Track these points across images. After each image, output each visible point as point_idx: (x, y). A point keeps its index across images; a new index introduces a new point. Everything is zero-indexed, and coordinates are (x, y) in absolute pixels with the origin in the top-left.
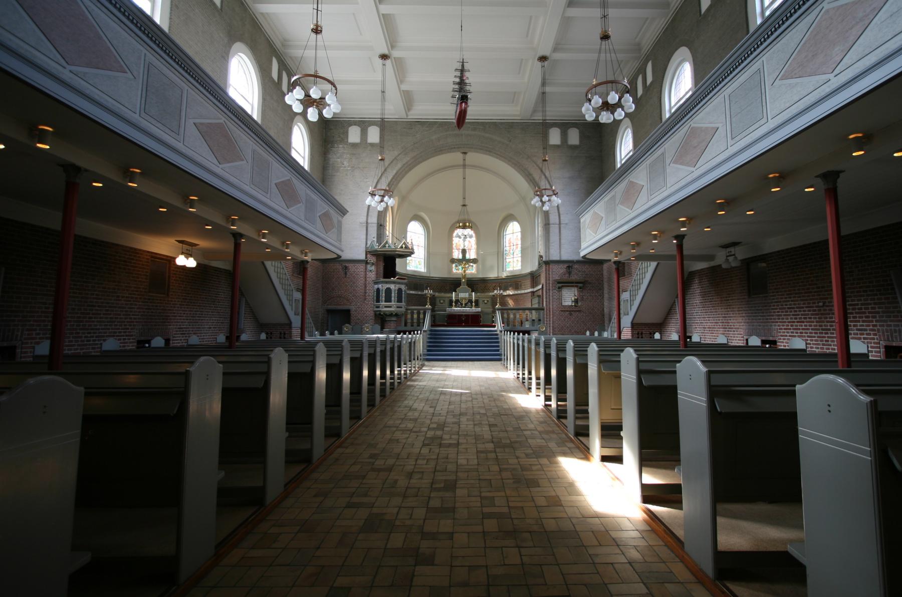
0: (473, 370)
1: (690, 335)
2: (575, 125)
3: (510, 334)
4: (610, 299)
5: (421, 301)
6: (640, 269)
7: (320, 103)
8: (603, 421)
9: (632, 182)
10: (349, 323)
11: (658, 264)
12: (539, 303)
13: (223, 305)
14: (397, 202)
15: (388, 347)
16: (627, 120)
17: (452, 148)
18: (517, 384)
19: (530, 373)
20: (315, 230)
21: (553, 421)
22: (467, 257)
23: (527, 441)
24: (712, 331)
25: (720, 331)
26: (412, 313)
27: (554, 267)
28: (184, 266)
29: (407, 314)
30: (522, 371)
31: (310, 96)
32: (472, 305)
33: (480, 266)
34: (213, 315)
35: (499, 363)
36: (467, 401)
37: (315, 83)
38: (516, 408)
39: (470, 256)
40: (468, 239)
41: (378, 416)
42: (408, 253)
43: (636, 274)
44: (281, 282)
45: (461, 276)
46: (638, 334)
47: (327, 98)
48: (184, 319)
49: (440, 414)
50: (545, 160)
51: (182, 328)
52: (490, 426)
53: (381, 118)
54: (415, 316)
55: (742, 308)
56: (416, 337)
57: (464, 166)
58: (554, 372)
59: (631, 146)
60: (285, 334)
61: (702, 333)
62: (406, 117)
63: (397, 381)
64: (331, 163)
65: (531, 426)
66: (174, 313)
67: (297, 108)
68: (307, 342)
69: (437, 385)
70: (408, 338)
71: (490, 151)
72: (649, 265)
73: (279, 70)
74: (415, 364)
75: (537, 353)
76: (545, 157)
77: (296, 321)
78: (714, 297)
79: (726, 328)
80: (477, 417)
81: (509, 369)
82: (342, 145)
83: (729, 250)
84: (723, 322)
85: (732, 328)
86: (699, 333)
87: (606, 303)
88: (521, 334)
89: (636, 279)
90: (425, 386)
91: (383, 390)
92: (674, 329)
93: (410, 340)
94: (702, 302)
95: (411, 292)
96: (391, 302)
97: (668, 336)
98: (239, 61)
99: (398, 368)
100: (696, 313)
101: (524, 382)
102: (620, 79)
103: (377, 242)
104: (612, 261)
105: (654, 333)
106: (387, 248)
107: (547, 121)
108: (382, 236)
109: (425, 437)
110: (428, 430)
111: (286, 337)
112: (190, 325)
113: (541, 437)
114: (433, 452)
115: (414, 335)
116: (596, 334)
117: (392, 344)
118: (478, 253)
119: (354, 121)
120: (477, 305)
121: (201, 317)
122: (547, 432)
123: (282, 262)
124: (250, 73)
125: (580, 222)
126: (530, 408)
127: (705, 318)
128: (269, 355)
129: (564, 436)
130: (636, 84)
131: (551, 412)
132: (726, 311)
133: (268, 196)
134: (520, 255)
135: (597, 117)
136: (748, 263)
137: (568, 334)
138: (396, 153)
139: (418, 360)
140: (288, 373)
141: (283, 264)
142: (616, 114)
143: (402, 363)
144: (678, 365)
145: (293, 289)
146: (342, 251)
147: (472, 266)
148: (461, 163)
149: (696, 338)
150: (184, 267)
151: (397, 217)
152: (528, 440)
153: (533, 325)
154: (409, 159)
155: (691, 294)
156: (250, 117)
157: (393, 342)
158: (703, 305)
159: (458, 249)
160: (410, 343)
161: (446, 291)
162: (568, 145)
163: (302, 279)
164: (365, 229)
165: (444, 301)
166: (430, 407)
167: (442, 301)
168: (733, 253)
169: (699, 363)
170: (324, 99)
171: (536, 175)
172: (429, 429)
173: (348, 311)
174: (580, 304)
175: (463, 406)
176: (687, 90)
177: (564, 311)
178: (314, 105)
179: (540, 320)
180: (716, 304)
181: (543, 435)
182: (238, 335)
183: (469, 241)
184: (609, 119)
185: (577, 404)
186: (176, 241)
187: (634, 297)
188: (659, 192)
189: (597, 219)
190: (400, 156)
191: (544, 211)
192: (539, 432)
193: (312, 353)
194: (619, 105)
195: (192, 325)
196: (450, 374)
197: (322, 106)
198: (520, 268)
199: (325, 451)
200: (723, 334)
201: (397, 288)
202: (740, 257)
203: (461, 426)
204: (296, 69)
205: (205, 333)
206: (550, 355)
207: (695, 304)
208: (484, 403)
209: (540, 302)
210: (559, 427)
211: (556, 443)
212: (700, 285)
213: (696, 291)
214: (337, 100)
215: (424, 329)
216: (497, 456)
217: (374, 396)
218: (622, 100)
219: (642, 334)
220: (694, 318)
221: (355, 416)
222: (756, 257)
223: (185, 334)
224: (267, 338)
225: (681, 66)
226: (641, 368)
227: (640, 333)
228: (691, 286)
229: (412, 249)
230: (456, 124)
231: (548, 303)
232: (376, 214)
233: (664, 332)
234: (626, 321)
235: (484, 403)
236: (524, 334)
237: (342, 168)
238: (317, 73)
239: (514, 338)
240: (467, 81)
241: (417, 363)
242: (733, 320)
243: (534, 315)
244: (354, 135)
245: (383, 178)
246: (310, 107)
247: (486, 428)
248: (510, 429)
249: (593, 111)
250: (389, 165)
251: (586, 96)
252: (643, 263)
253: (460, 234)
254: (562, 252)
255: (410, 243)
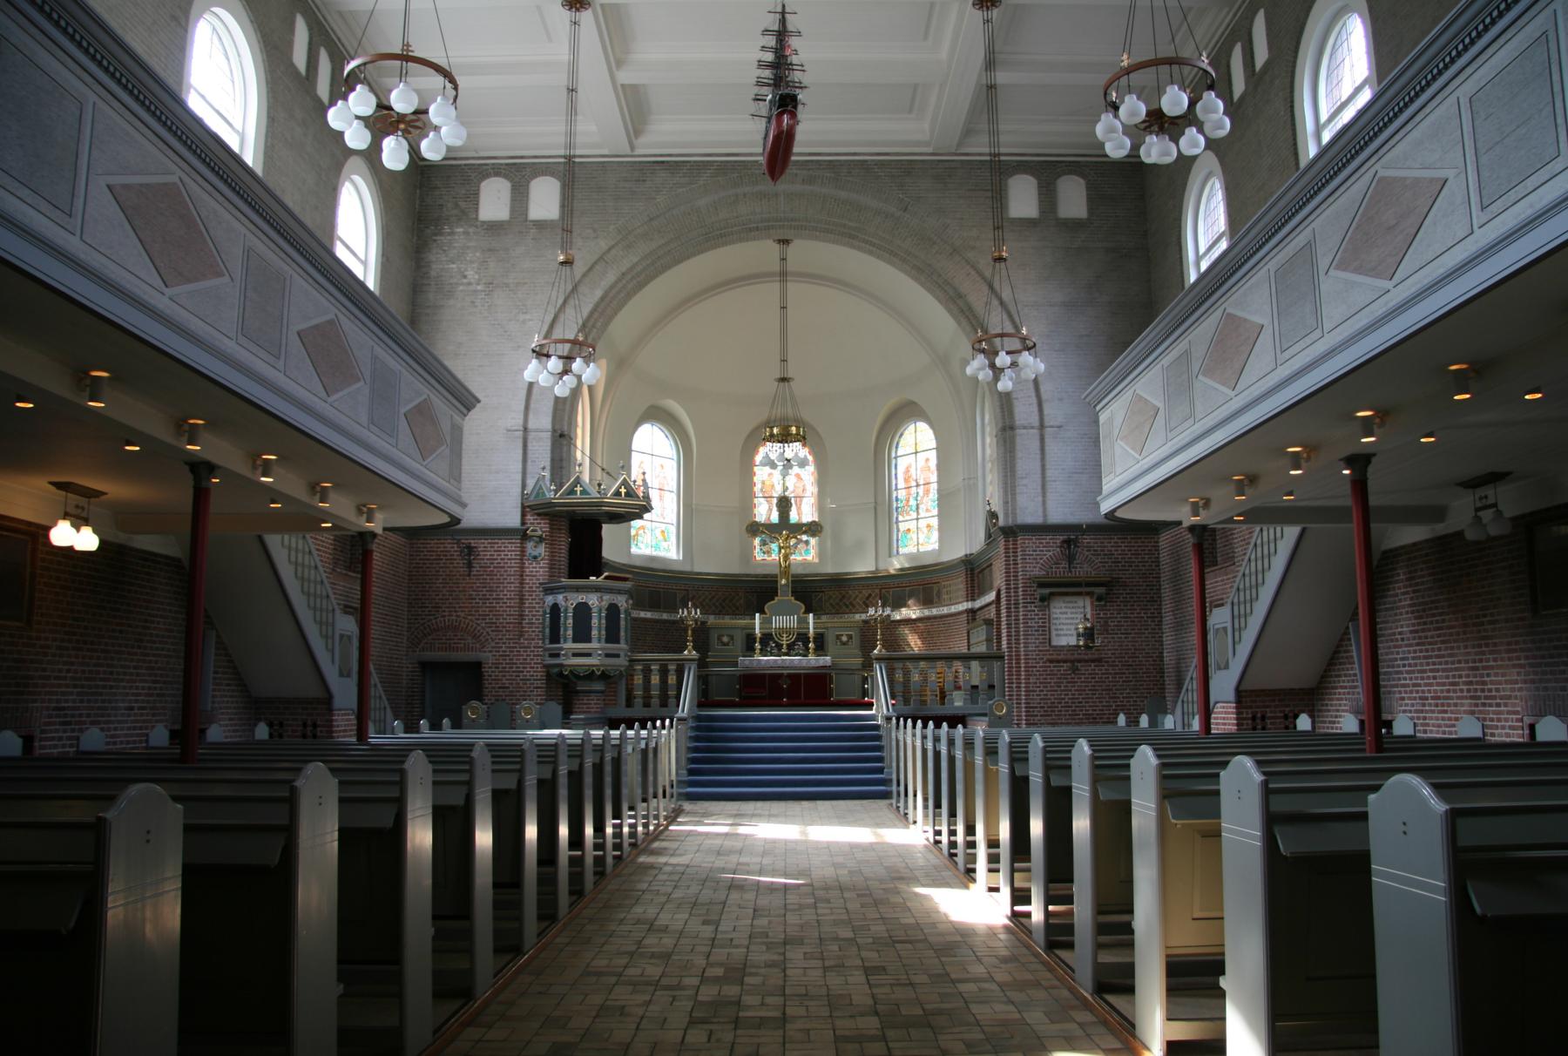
0: (796, 842)
1: (1390, 718)
2: (1074, 168)
3: (914, 727)
4: (1179, 626)
5: (670, 636)
6: (1256, 545)
7: (414, 125)
8: (1170, 952)
9: (1230, 318)
10: (479, 697)
11: (1304, 530)
12: (989, 640)
13: (163, 649)
14: (605, 372)
15: (589, 763)
16: (1210, 155)
17: (751, 230)
18: (934, 859)
19: (970, 830)
20: (395, 450)
21: (1037, 955)
22: (794, 517)
23: (968, 1008)
24: (1443, 705)
25: (1462, 705)
26: (647, 672)
27: (1027, 543)
28: (71, 548)
29: (632, 675)
30: (949, 825)
31: (390, 108)
32: (808, 649)
33: (829, 543)
34: (138, 675)
35: (883, 803)
36: (801, 907)
37: (402, 75)
38: (934, 923)
39: (799, 514)
40: (796, 470)
41: (567, 944)
42: (635, 507)
43: (1247, 558)
44: (306, 589)
45: (776, 571)
46: (1254, 718)
47: (432, 110)
48: (67, 686)
49: (732, 940)
50: (1000, 259)
51: (64, 709)
52: (868, 971)
53: (565, 157)
54: (655, 679)
55: (1517, 643)
56: (659, 735)
57: (783, 275)
58: (1037, 827)
59: (1221, 223)
60: (315, 726)
61: (1416, 711)
62: (629, 152)
63: (611, 853)
64: (433, 273)
65: (979, 970)
66: (44, 670)
67: (357, 138)
68: (376, 747)
69: (720, 863)
70: (638, 738)
71: (852, 237)
72: (1279, 534)
73: (310, 44)
74: (657, 809)
75: (990, 778)
76: (1000, 251)
77: (345, 693)
78: (1447, 617)
79: (1479, 698)
80: (830, 948)
81: (911, 820)
82: (462, 226)
83: (1481, 492)
84: (1471, 683)
85: (1494, 697)
86: (1410, 711)
87: (1168, 638)
88: (945, 725)
89: (1247, 572)
90: (688, 866)
91: (576, 877)
92: (1345, 704)
93: (643, 745)
94: (1416, 631)
95: (643, 614)
96: (589, 640)
97: (1330, 722)
98: (214, 29)
99: (614, 818)
100: (1402, 659)
101: (952, 855)
102: (1187, 52)
103: (552, 481)
104: (1186, 524)
105: (1296, 716)
106: (578, 498)
107: (1002, 158)
108: (565, 464)
109: (696, 1000)
110: (701, 982)
111: (319, 734)
112: (82, 701)
113: (1005, 999)
114: (718, 1041)
115: (655, 732)
116: (1144, 721)
117: (599, 754)
118: (821, 508)
119: (493, 164)
120: (821, 648)
121: (108, 680)
122: (1021, 986)
123: (308, 536)
124: (239, 55)
125: (1097, 422)
126: (971, 925)
127: (1424, 671)
128: (294, 781)
129: (1065, 993)
130: (1228, 66)
131: (1030, 932)
132: (1476, 654)
133: (280, 364)
134: (935, 512)
135: (1135, 147)
136: (1529, 525)
137: (1068, 724)
138: (603, 244)
139: (664, 796)
140: (340, 830)
141: (310, 541)
142: (1183, 141)
143: (625, 806)
144: (1372, 797)
145: (336, 607)
146: (464, 505)
147: (807, 543)
148: (777, 269)
149: (1402, 727)
150: (69, 551)
151: (605, 415)
152: (971, 1006)
153: (974, 701)
154: (635, 260)
155: (1387, 610)
156: (237, 159)
157: (600, 749)
158: (1420, 638)
159: (768, 498)
160: (645, 752)
161: (736, 612)
162: (1057, 219)
163: (359, 581)
164: (520, 445)
165: (732, 638)
166: (705, 923)
167: (725, 639)
168: (1491, 501)
169: (1426, 791)
170: (426, 112)
171: (977, 297)
172: (704, 980)
173: (476, 668)
174: (1098, 642)
175: (792, 919)
176: (1358, 83)
177: (1058, 661)
178: (398, 129)
179: (992, 687)
180: (1451, 635)
181: (1008, 994)
182: (203, 727)
183: (798, 476)
184: (1168, 154)
185: (1100, 909)
186: (51, 483)
187: (1243, 620)
188: (1302, 344)
189: (1145, 415)
190: (613, 252)
191: (1000, 393)
192: (1000, 985)
193: (398, 779)
194: (1190, 118)
195: (89, 701)
196: (751, 835)
197: (418, 131)
198: (936, 546)
199: (435, 1032)
200: (1472, 713)
201: (605, 604)
202: (1509, 511)
203: (789, 972)
204: (356, 45)
205: (119, 722)
206: (1026, 779)
207: (1399, 637)
208: (847, 912)
209: (993, 638)
210: (1051, 970)
211: (1045, 1013)
212: (1410, 586)
213: (1400, 601)
214: (457, 117)
215: (680, 714)
216: (889, 1049)
217: (555, 893)
218: (1199, 106)
219: (1263, 718)
220: (1398, 673)
221: (508, 945)
222: (1548, 510)
223: (69, 723)
224: (271, 735)
225: (1341, 23)
226: (1273, 808)
227: (1259, 715)
228: (1389, 590)
229: (647, 498)
230: (765, 167)
231: (1014, 638)
232: (550, 404)
233: (1320, 711)
234: (1224, 685)
235: (847, 912)
236: (952, 726)
237: (461, 288)
238: (408, 50)
239: (924, 737)
240: (794, 59)
241: (662, 806)
242: (1496, 675)
243: (976, 674)
244: (494, 201)
245: (569, 311)
246: (388, 135)
247: (858, 978)
248: (921, 978)
249: (1124, 133)
250: (584, 275)
251: (1105, 94)
252: (1265, 528)
253: (773, 456)
254: (1050, 505)
255: (639, 482)
